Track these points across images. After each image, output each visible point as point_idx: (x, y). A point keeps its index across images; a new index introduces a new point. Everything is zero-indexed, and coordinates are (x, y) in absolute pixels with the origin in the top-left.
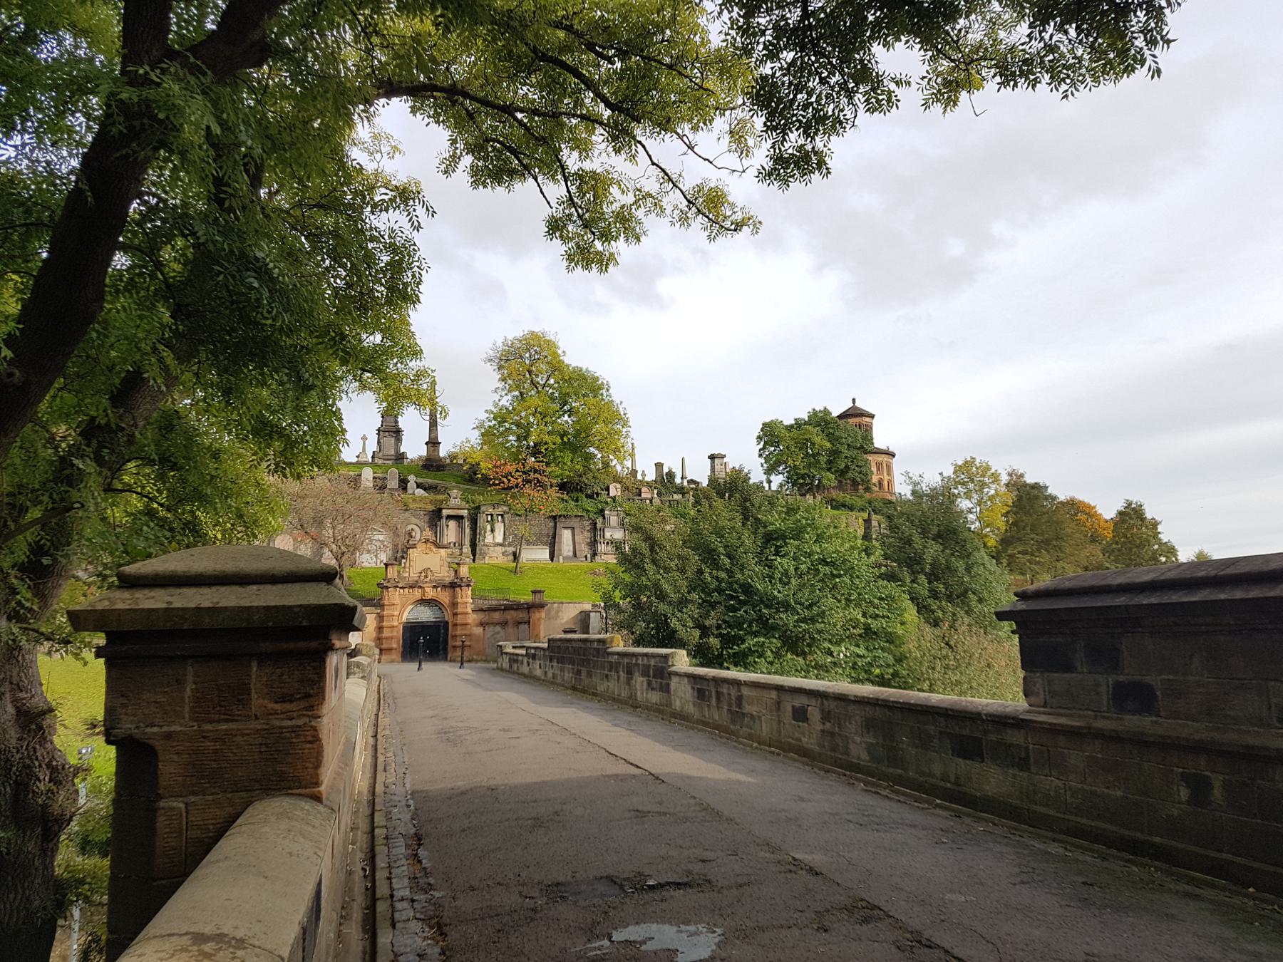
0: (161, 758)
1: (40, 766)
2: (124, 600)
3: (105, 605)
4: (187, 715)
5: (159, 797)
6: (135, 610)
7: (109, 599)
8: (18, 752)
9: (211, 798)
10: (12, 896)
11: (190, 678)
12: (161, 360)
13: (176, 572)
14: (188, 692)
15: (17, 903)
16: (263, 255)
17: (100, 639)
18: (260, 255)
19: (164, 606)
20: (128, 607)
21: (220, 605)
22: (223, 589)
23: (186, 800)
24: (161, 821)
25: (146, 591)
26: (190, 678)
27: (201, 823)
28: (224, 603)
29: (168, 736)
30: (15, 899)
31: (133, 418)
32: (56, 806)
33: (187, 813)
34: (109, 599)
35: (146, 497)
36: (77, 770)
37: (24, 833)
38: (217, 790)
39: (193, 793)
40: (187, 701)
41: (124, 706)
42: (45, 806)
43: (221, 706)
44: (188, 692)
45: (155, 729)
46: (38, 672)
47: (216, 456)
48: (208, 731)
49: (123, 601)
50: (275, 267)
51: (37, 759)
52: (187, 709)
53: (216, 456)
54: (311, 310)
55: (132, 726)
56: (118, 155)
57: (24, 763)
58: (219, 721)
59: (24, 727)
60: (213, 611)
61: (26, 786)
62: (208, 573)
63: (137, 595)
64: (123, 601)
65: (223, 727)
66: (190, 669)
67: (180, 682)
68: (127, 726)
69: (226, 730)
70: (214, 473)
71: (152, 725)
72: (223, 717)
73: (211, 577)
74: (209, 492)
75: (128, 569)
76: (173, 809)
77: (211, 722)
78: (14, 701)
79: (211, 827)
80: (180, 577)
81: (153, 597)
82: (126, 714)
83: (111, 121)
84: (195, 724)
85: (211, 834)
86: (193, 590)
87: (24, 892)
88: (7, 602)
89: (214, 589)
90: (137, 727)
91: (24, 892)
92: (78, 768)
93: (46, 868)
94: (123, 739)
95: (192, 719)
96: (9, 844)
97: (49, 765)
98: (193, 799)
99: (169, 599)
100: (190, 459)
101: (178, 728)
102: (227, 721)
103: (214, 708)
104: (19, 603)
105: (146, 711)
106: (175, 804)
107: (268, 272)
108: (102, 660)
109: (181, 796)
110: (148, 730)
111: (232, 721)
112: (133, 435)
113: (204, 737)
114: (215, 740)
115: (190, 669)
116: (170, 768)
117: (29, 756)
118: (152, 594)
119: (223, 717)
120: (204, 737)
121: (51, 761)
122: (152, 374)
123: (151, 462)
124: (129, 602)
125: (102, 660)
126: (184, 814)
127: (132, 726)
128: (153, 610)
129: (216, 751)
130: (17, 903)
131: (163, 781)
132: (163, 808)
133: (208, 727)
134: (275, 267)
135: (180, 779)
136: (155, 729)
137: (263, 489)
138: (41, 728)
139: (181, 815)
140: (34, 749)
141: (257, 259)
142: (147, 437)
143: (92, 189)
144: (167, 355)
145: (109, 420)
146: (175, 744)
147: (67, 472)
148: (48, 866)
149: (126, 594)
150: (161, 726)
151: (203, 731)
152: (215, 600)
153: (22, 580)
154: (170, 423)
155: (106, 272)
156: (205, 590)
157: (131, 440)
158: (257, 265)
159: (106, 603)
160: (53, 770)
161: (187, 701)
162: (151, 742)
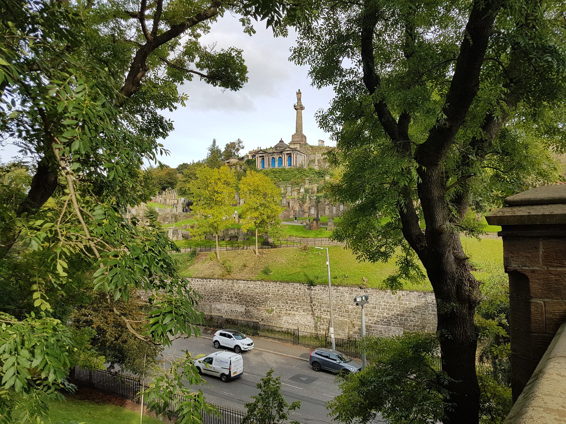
0: (531, 281)
1: (465, 280)
2: (509, 212)
3: (500, 214)
4: (541, 263)
5: (531, 297)
6: (514, 216)
7: (502, 212)
8: (456, 273)
9: (556, 301)
10: (460, 329)
11: (541, 246)
12: (501, 107)
13: (531, 199)
14: (541, 253)
15: (462, 332)
16: (553, 44)
17: (499, 228)
18: (551, 44)
19: (527, 214)
20: (511, 215)
21: (554, 213)
22: (554, 206)
23: (543, 300)
24: (533, 309)
25: (518, 208)
26: (541, 246)
27: (552, 311)
28: (556, 212)
29: (533, 271)
30: (461, 330)
31: (491, 135)
32: (473, 297)
33: (545, 306)
34: (502, 212)
35: (496, 169)
36: (480, 283)
37: (462, 305)
38: (558, 297)
39: (547, 298)
40: (541, 256)
41: (512, 257)
42: (469, 296)
43: (557, 260)
44: (541, 253)
45: (527, 268)
46: (460, 243)
47: (526, 147)
48: (552, 271)
49: (508, 212)
50: (560, 48)
51: (464, 277)
52: (541, 260)
53: (526, 147)
54: (83, 196)
55: (517, 266)
56: (483, 18)
57: (459, 278)
58: (557, 267)
59: (458, 264)
60: (551, 216)
61: (461, 287)
62: (546, 199)
63: (514, 210)
64: (508, 212)
65: (559, 269)
66: (541, 243)
67: (537, 248)
68: (514, 266)
69: (561, 271)
70: (526, 155)
71: (525, 266)
72: (559, 265)
73: (547, 200)
74: (525, 164)
75: (509, 198)
76: (538, 303)
77: (553, 267)
78: (454, 253)
79: (557, 314)
80: (533, 201)
81: (521, 210)
82: (513, 261)
83: (478, 4)
84: (545, 267)
85: (557, 317)
86: (539, 207)
87: (464, 329)
88: (449, 215)
89: (549, 206)
90: (519, 267)
91: (464, 329)
92: (480, 282)
93: (471, 320)
94: (513, 271)
95: (544, 265)
96: (457, 308)
97: (469, 280)
98: (547, 300)
99: (529, 211)
100: (515, 149)
101: (538, 268)
102: (560, 267)
103: (554, 260)
104: (453, 215)
105: (522, 260)
106: (539, 301)
107: (556, 52)
108: (501, 238)
109: (541, 298)
110: (524, 268)
111: (563, 267)
112: (491, 142)
113: (550, 273)
114: (555, 275)
115: (541, 243)
116: (535, 286)
117: (461, 276)
118: (520, 209)
119: (559, 265)
120: (550, 273)
121: (469, 278)
122: (498, 114)
123: (498, 153)
124: (511, 212)
125: (501, 238)
126: (544, 306)
127: (517, 266)
128: (522, 216)
129: (556, 280)
130: (462, 332)
131: (532, 291)
132: (534, 303)
133: (551, 269)
134: (560, 48)
135: (540, 290)
136: (527, 268)
137: (550, 160)
138: (464, 265)
139: (542, 307)
140: (463, 273)
141: (550, 47)
142: (495, 142)
143: (472, 38)
144: (504, 104)
145: (482, 137)
146: (536, 275)
147: (467, 161)
148: (472, 320)
149: (509, 209)
150: (529, 267)
151: (550, 271)
152: (551, 211)
153: (454, 206)
154: (504, 135)
155: (479, 74)
156: (545, 207)
157: (490, 144)
158: (551, 49)
159: (501, 213)
160: (471, 282)
161: (541, 256)
162: (525, 273)
